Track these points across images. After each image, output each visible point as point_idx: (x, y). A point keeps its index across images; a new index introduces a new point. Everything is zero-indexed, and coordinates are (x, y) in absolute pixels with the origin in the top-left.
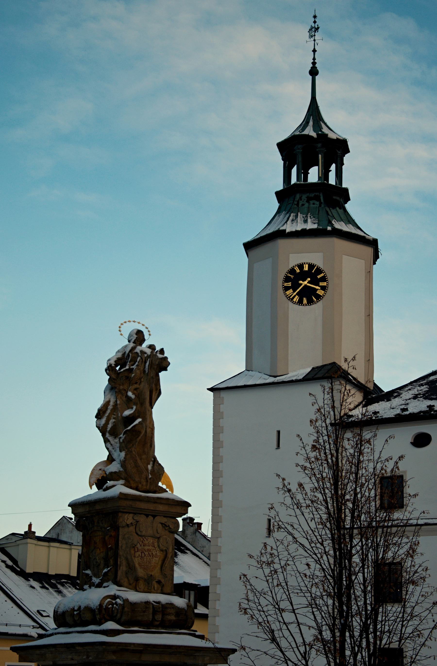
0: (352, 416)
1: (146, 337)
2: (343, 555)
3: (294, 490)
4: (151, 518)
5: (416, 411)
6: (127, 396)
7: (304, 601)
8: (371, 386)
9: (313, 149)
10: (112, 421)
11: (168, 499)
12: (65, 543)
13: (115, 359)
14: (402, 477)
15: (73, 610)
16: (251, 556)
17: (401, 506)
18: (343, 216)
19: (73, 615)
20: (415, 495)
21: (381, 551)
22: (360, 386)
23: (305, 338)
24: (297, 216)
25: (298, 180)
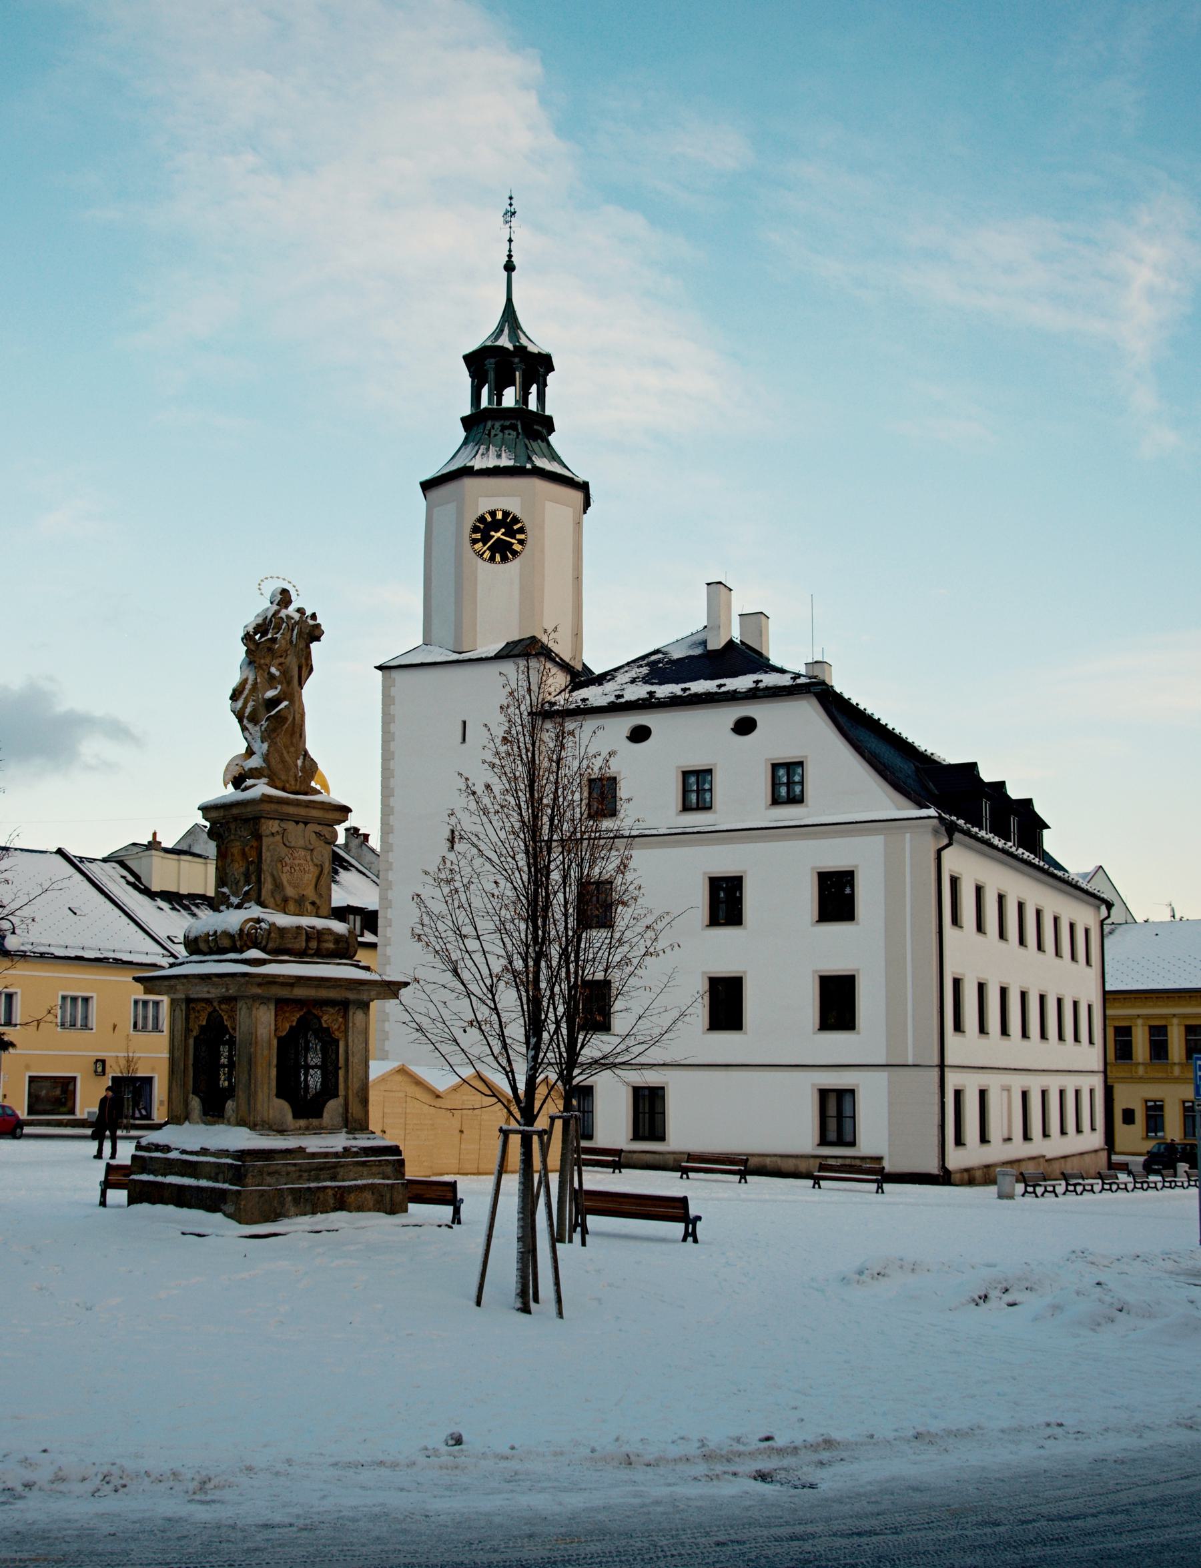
0: (555, 704)
1: (293, 597)
2: (539, 874)
3: (479, 793)
4: (301, 825)
5: (633, 698)
6: (269, 673)
7: (491, 926)
8: (579, 668)
9: (510, 364)
10: (251, 704)
11: (323, 803)
12: (199, 856)
13: (254, 625)
14: (615, 779)
15: (208, 935)
16: (426, 873)
17: (613, 813)
18: (546, 451)
19: (207, 941)
20: (629, 800)
21: (586, 866)
22: (565, 667)
23: (498, 601)
24: (488, 449)
25: (489, 403)
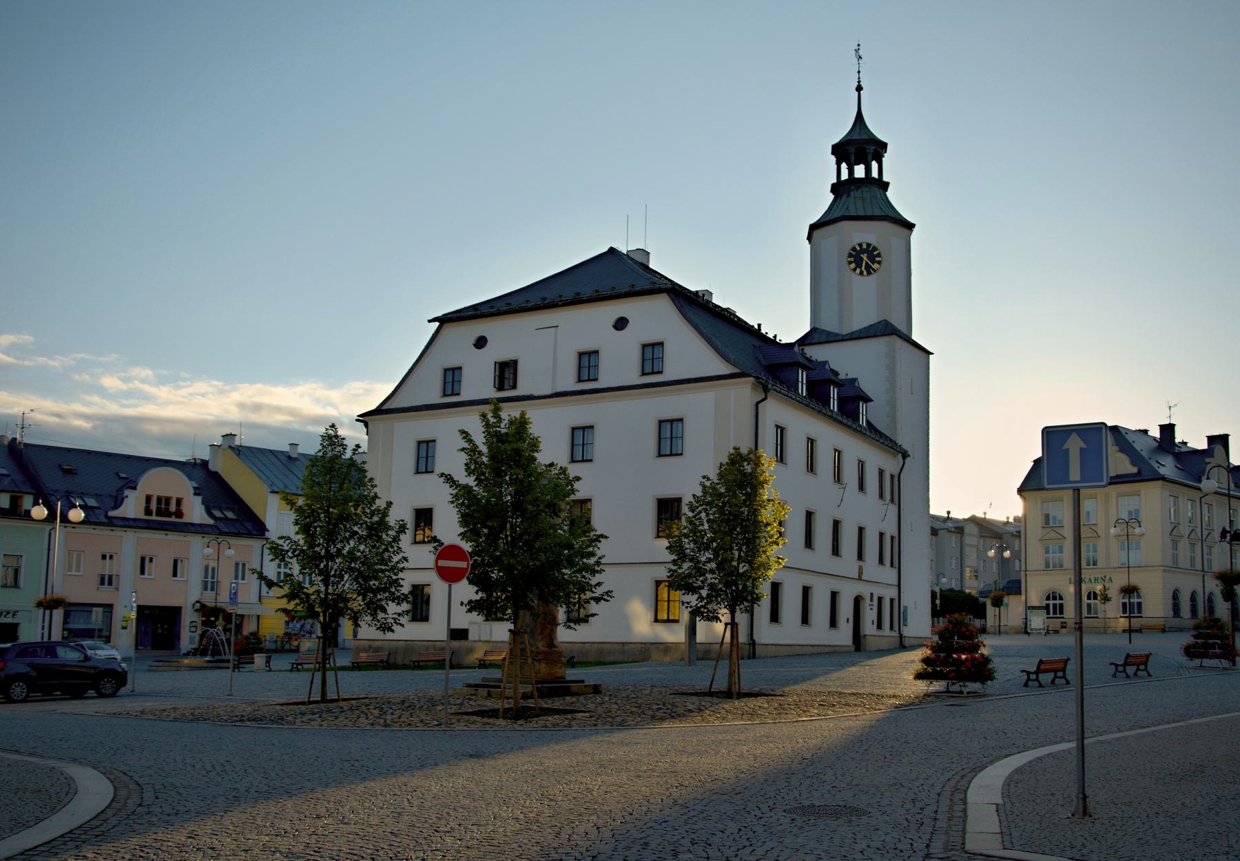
9: (859, 147)
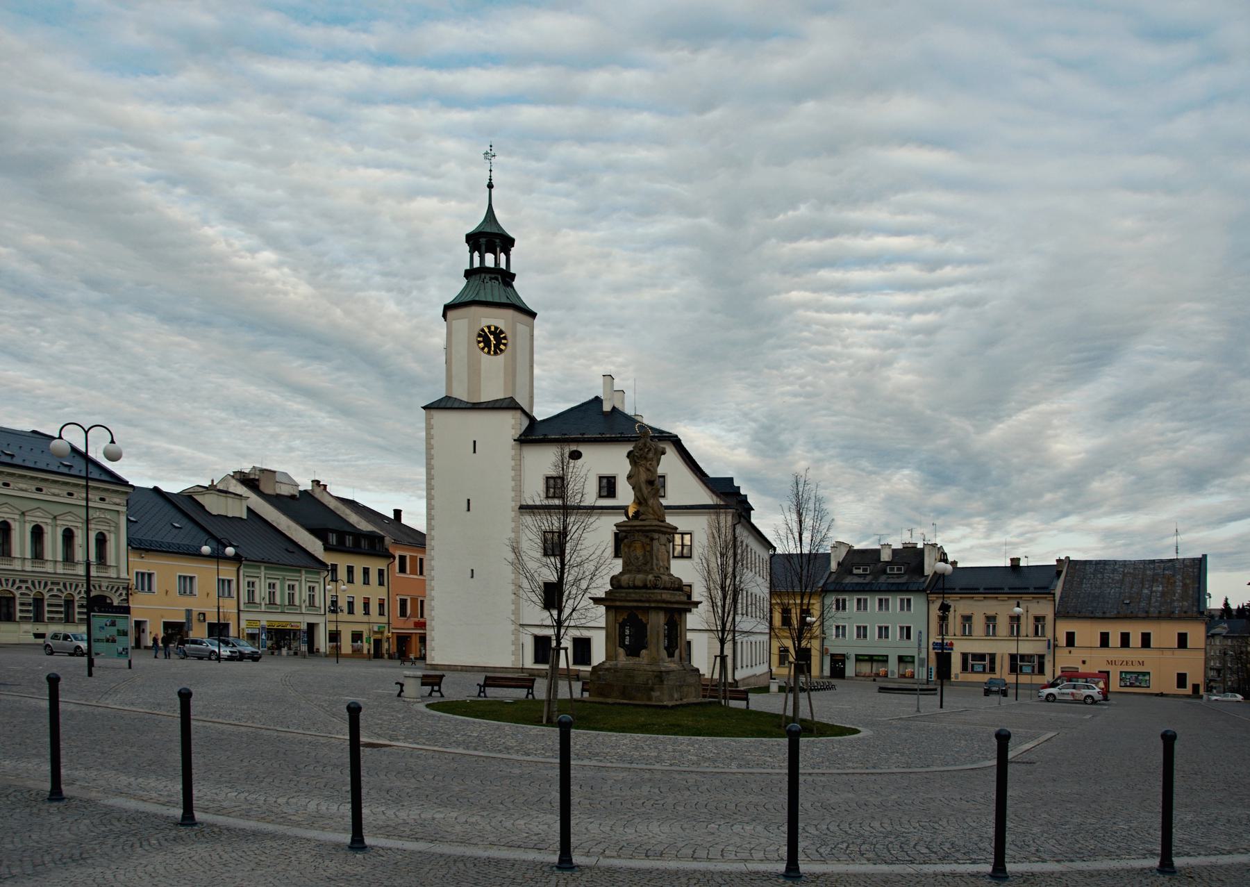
9: (489, 238)
